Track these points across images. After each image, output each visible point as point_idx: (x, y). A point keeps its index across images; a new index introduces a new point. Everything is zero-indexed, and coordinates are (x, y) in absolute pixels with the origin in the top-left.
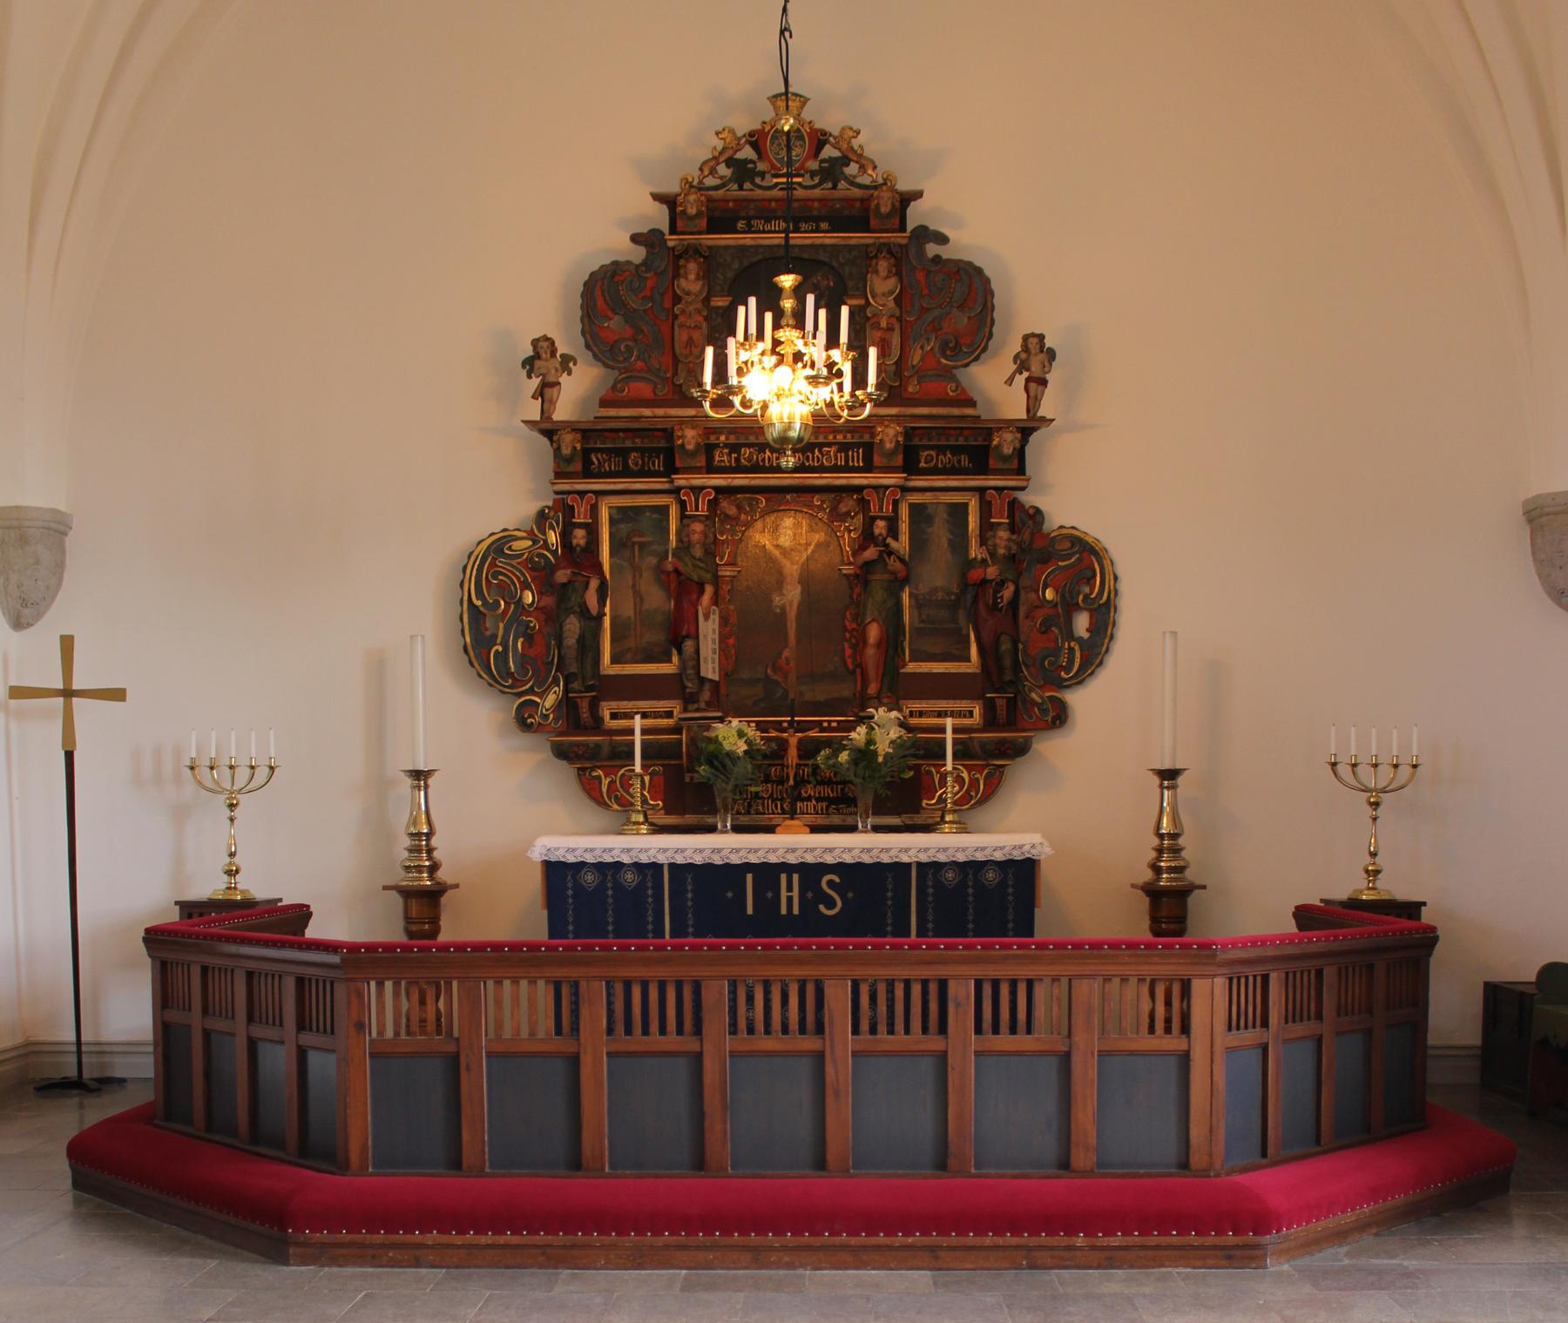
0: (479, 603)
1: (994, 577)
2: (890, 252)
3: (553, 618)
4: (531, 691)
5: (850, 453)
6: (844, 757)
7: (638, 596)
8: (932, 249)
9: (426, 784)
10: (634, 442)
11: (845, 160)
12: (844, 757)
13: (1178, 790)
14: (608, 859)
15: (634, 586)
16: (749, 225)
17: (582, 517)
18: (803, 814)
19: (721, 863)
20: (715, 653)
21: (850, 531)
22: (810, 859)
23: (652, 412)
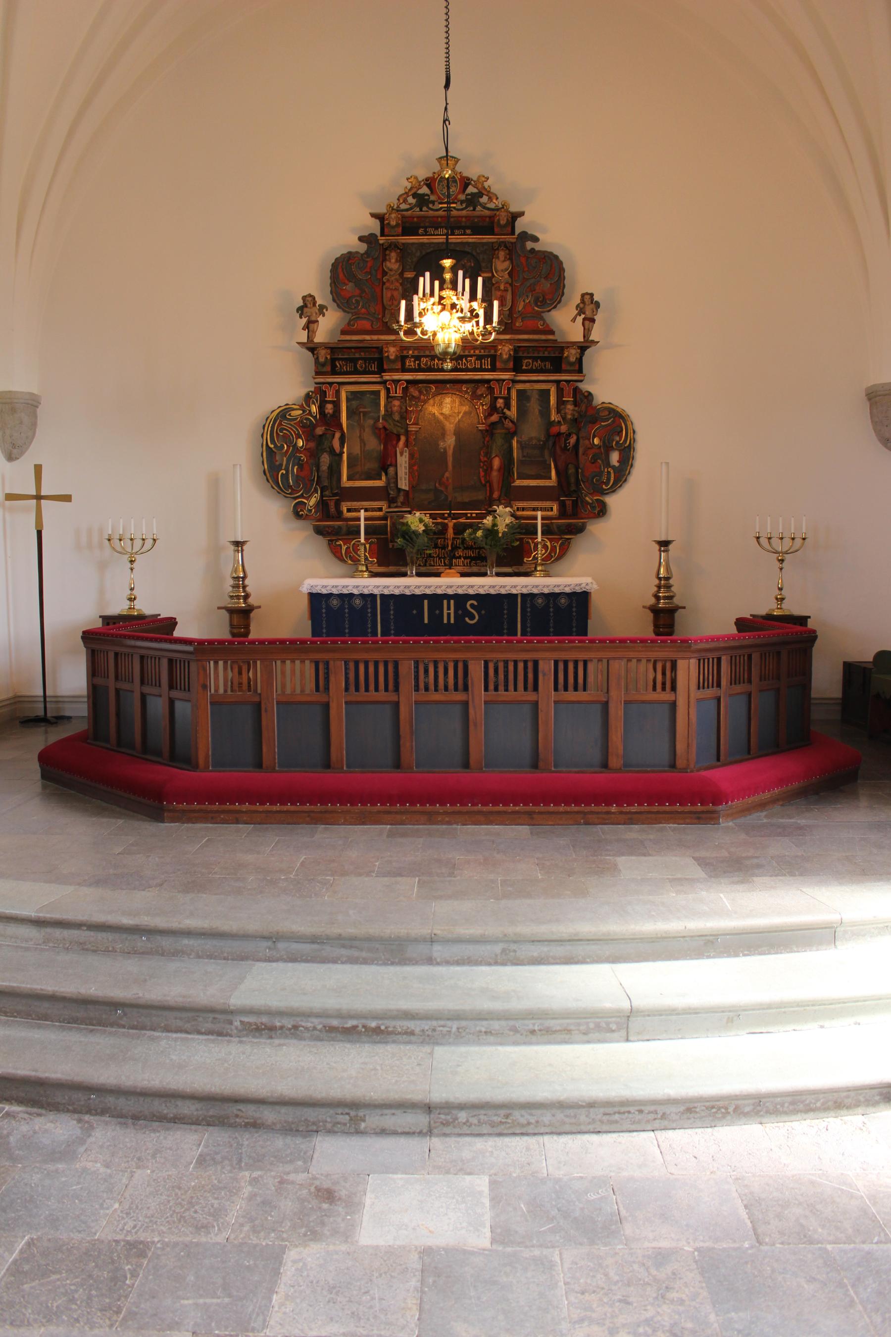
0: (272, 446)
2: (506, 246)
3: (314, 454)
4: (302, 496)
6: (480, 533)
7: (363, 442)
8: (529, 245)
9: (242, 549)
10: (360, 355)
11: (480, 194)
12: (480, 533)
14: (345, 591)
15: (360, 436)
21: (483, 405)
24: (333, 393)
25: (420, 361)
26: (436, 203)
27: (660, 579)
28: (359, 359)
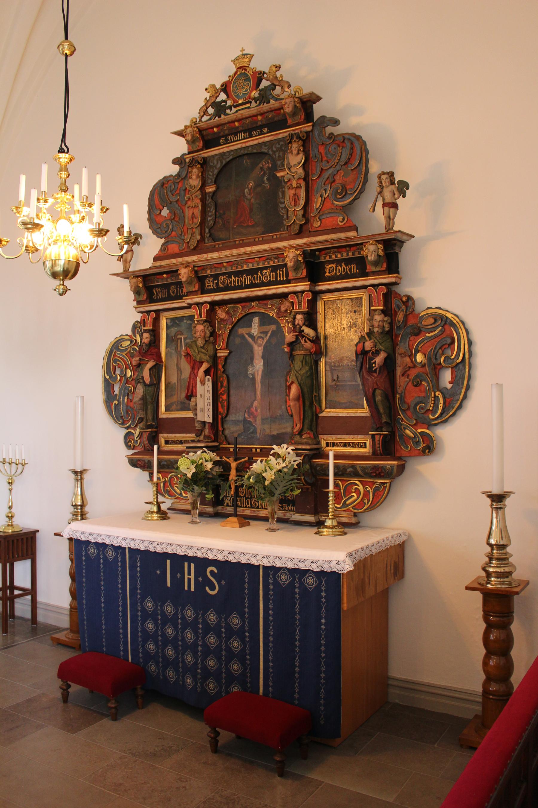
1: (369, 349)
2: (299, 138)
5: (278, 272)
8: (329, 129)
10: (172, 280)
13: (507, 509)
15: (177, 364)
17: (148, 326)
18: (263, 508)
20: (210, 405)
21: (288, 323)
22: (200, 555)
24: (150, 322)
25: (218, 280)
27: (491, 545)
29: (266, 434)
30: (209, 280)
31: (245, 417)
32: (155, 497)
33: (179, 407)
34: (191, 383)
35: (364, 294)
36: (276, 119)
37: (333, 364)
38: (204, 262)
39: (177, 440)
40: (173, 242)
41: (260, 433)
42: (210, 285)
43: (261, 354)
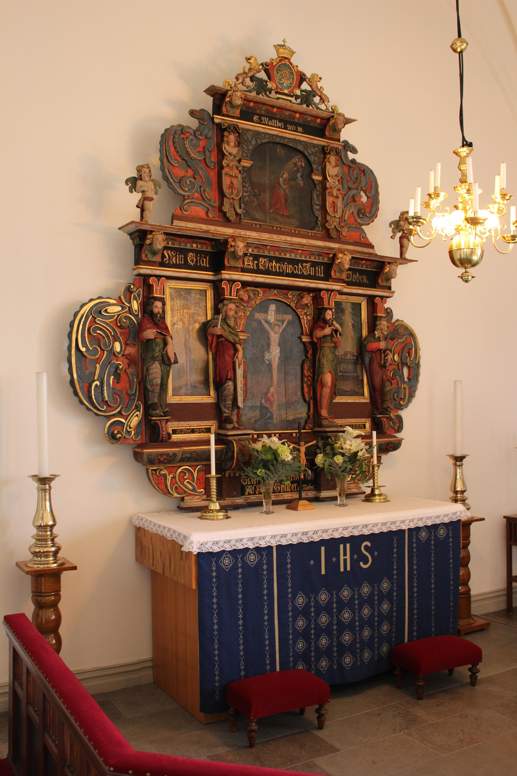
0: (83, 349)
4: (120, 414)
5: (317, 268)
8: (351, 156)
9: (50, 486)
14: (240, 547)
16: (260, 119)
17: (158, 293)
18: (284, 492)
19: (308, 541)
21: (307, 315)
23: (207, 228)
25: (258, 261)
26: (273, 92)
27: (456, 492)
28: (192, 251)
29: (282, 419)
30: (248, 259)
31: (261, 404)
32: (376, 481)
33: (189, 392)
34: (401, 372)
35: (208, 288)
36: (312, 124)
37: (340, 357)
38: (255, 240)
39: (187, 429)
40: (199, 205)
41: (276, 419)
42: (250, 265)
43: (277, 342)
